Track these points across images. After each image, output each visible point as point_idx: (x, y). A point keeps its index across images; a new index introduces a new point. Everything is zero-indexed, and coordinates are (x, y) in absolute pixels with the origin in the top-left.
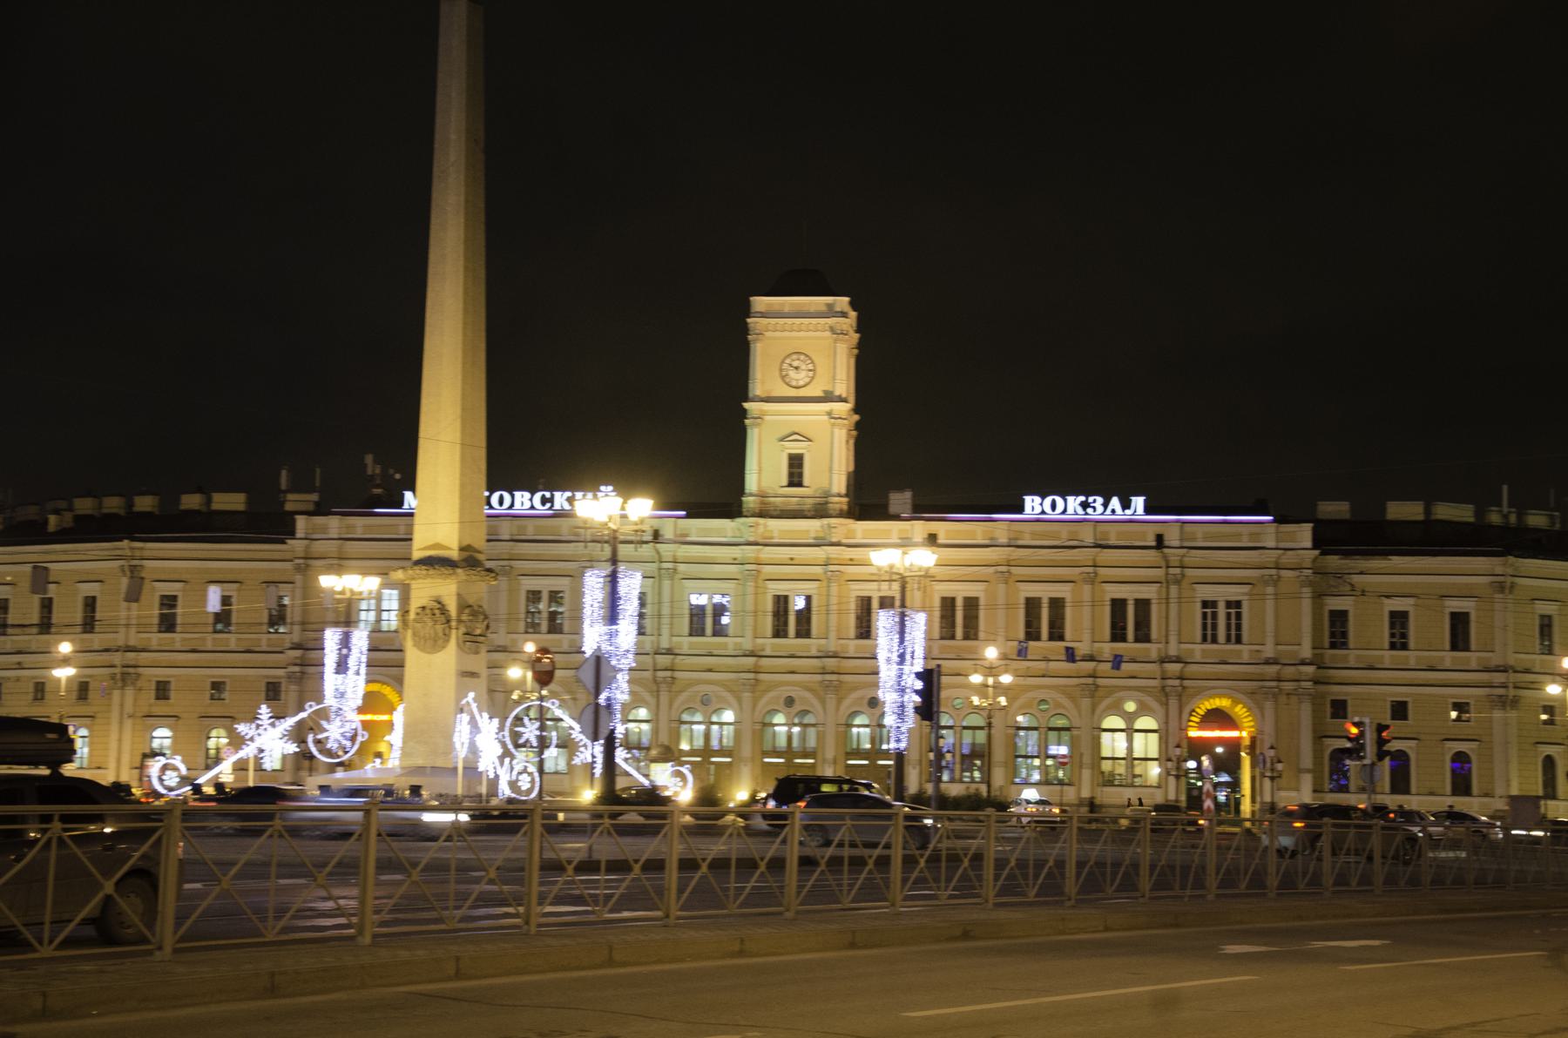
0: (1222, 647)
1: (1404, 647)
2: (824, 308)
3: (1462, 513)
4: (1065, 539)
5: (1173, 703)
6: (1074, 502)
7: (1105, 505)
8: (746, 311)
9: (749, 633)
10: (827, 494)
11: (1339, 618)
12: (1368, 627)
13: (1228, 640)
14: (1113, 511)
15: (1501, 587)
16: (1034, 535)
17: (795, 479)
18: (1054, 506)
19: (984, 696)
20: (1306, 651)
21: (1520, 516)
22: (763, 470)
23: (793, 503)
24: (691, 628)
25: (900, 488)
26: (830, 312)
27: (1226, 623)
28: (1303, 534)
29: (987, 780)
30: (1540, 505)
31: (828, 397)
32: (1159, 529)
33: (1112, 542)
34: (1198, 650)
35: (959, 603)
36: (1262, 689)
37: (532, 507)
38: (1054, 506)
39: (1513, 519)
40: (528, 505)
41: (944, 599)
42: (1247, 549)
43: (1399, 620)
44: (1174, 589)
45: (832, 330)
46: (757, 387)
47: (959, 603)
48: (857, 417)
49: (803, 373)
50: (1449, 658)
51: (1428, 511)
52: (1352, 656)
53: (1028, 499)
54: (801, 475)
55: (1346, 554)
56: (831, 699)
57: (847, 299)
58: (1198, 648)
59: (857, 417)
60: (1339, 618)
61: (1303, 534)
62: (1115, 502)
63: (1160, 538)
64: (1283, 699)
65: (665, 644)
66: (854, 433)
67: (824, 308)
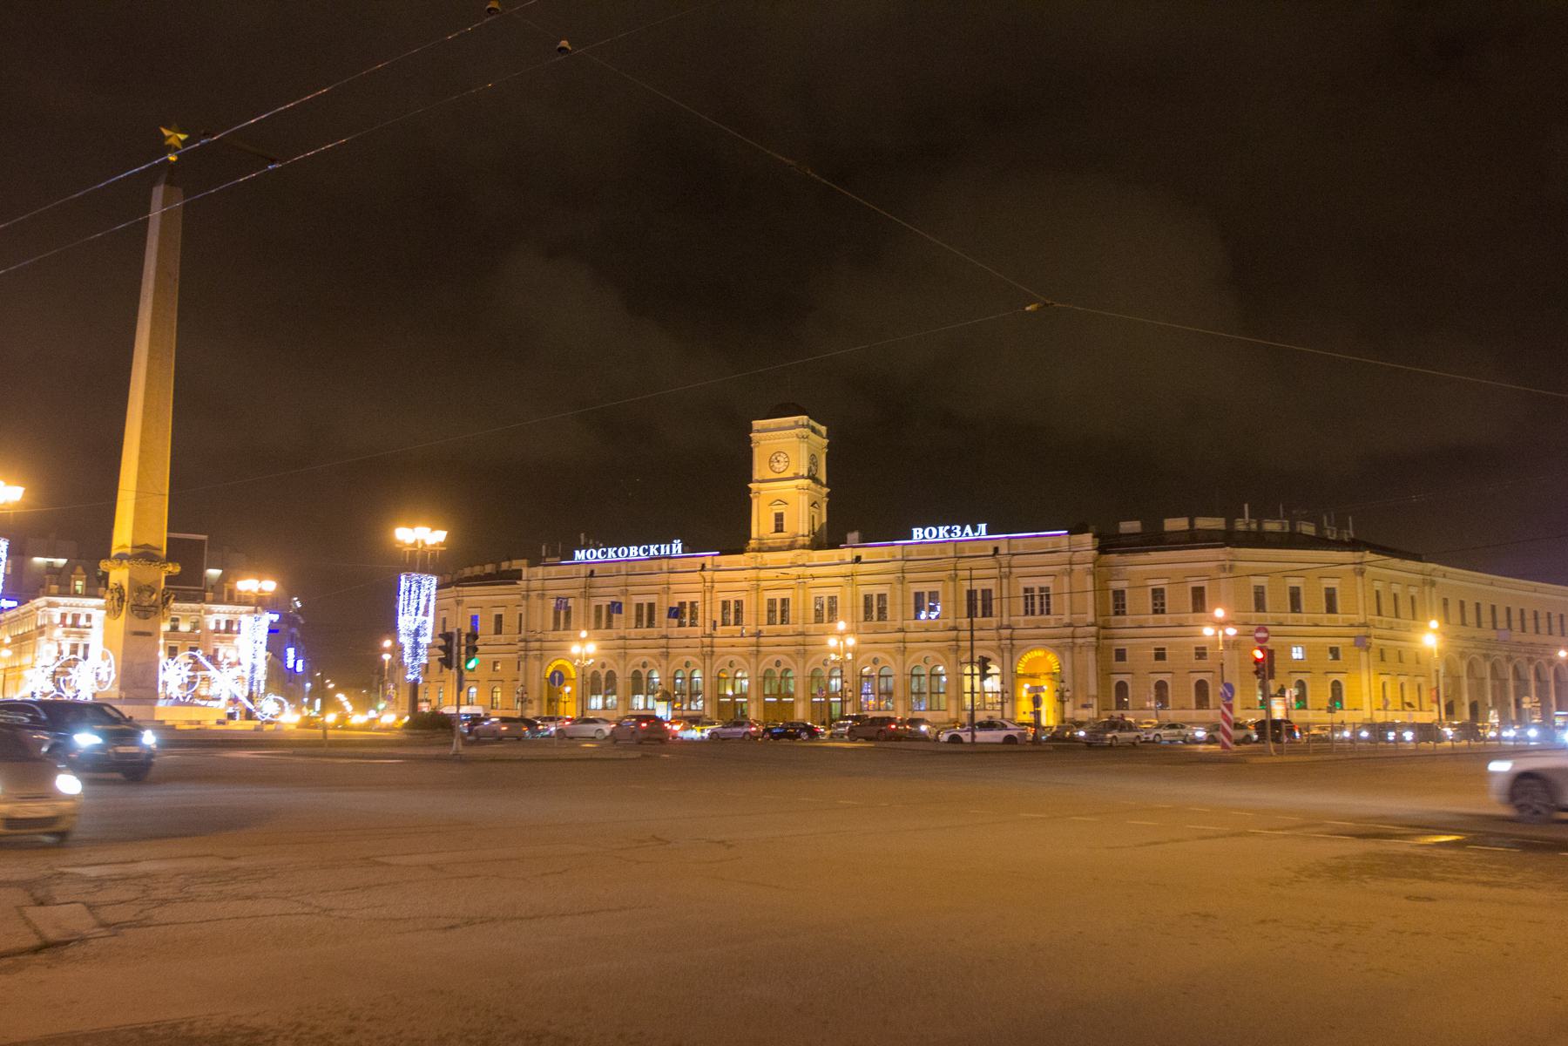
0: (1037, 617)
1: (1163, 612)
3: (1217, 523)
4: (931, 557)
5: (1007, 655)
6: (942, 530)
8: (750, 429)
9: (951, 616)
10: (797, 535)
11: (1119, 595)
12: (1138, 602)
13: (1042, 612)
15: (1223, 569)
17: (779, 528)
19: (837, 653)
20: (1090, 618)
21: (1260, 525)
22: (761, 524)
23: (778, 543)
25: (852, 531)
26: (797, 426)
27: (1035, 602)
28: (1087, 539)
29: (1008, 694)
30: (1274, 516)
31: (797, 477)
32: (995, 544)
34: (1022, 620)
36: (1066, 644)
39: (1254, 526)
42: (1055, 557)
43: (1158, 594)
44: (1005, 581)
49: (786, 465)
50: (1325, 618)
51: (1191, 524)
52: (1128, 620)
55: (1122, 553)
56: (801, 662)
58: (1022, 619)
61: (1087, 539)
62: (968, 529)
63: (996, 550)
64: (1077, 650)
65: (1005, 622)
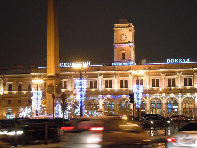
2: (128, 26)
7: (182, 60)
8: (114, 27)
14: (184, 62)
16: (153, 67)
18: (172, 61)
24: (168, 85)
25: (144, 59)
26: (129, 26)
31: (129, 42)
33: (120, 70)
35: (124, 81)
37: (170, 62)
38: (172, 61)
40: (169, 62)
41: (152, 80)
45: (129, 30)
46: (115, 41)
47: (124, 81)
48: (135, 46)
53: (167, 60)
54: (125, 57)
57: (132, 24)
59: (135, 46)
60: (20, 85)
66: (135, 49)
67: (128, 26)
